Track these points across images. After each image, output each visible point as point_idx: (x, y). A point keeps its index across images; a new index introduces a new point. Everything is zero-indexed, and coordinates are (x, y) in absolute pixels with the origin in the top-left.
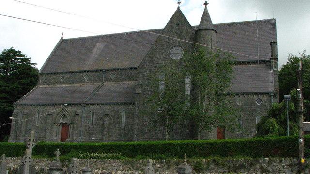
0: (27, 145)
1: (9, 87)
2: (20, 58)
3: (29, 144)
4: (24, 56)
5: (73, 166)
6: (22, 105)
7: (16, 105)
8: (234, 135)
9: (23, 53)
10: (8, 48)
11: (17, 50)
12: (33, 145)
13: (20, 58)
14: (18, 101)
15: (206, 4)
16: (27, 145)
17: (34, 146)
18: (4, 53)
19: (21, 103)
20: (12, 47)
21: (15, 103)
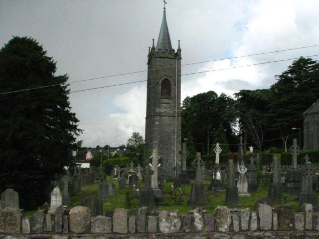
0: (291, 153)
1: (303, 97)
2: (312, 65)
3: (293, 152)
4: (315, 62)
5: (307, 169)
6: (312, 114)
7: (306, 115)
8: (199, 137)
9: (313, 60)
10: (297, 58)
11: (306, 58)
12: (297, 152)
13: (312, 65)
14: (307, 110)
15: (179, 41)
16: (291, 153)
17: (298, 154)
18: (294, 64)
19: (311, 112)
20: (302, 57)
21: (305, 113)
